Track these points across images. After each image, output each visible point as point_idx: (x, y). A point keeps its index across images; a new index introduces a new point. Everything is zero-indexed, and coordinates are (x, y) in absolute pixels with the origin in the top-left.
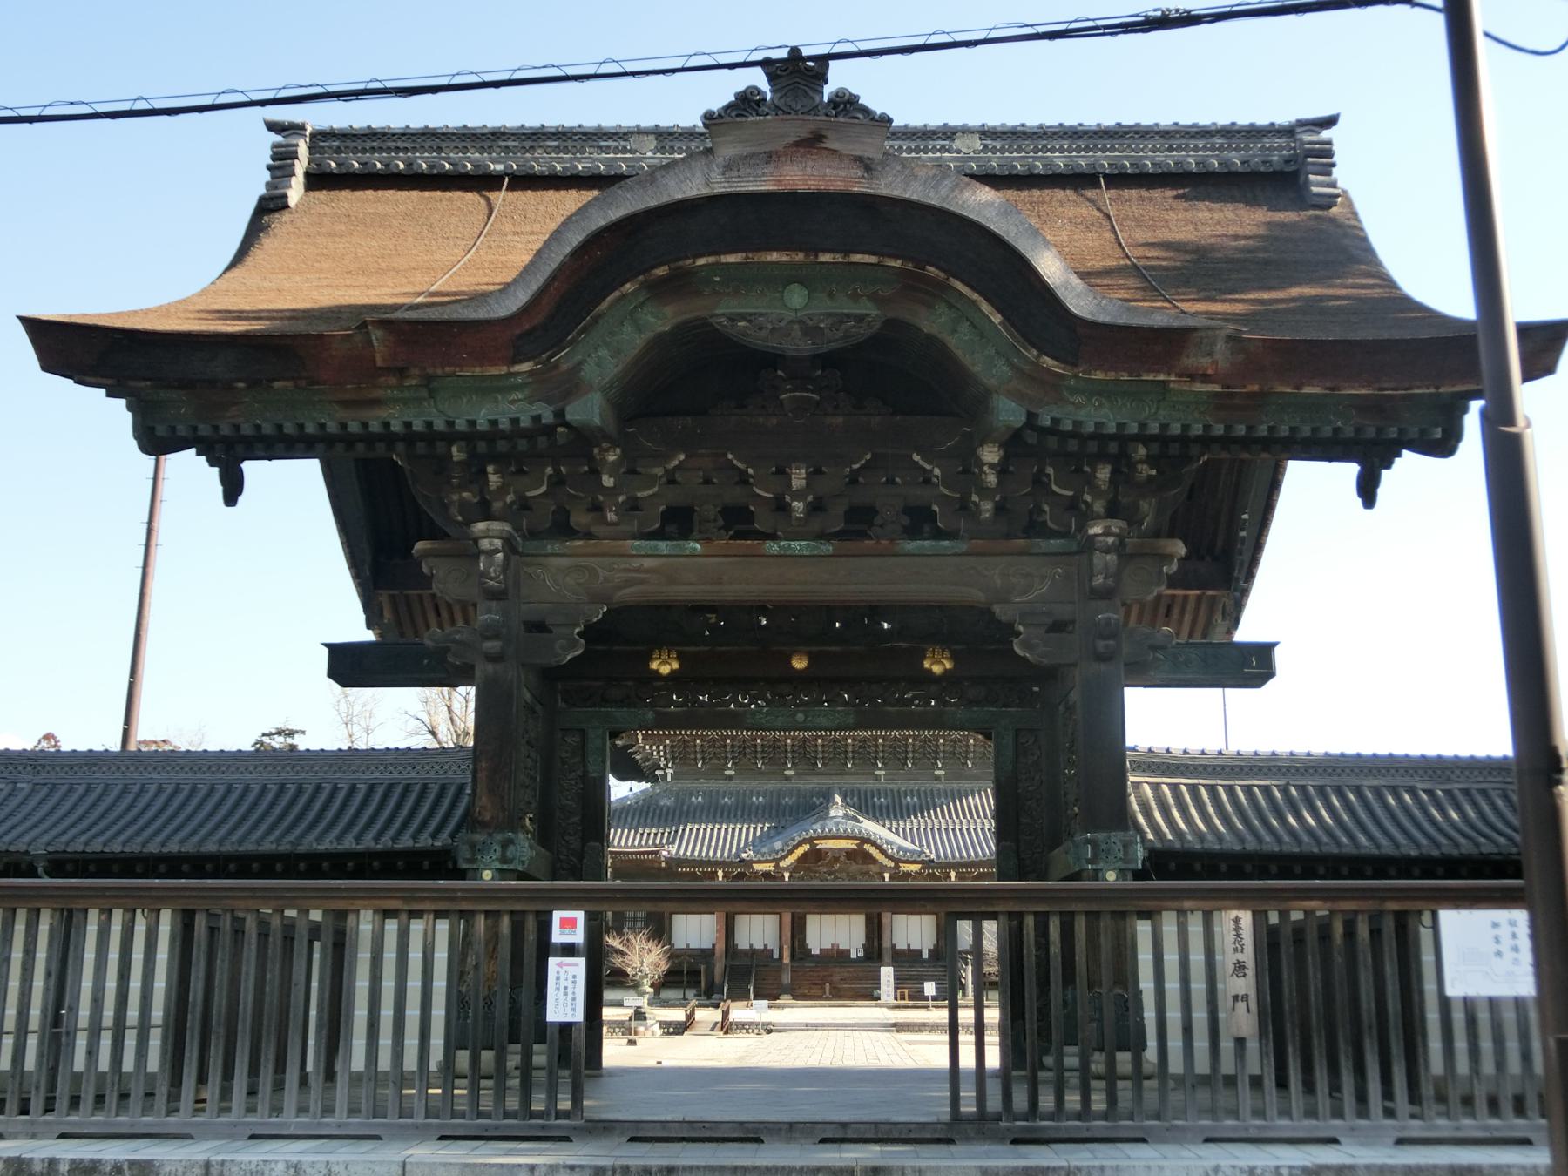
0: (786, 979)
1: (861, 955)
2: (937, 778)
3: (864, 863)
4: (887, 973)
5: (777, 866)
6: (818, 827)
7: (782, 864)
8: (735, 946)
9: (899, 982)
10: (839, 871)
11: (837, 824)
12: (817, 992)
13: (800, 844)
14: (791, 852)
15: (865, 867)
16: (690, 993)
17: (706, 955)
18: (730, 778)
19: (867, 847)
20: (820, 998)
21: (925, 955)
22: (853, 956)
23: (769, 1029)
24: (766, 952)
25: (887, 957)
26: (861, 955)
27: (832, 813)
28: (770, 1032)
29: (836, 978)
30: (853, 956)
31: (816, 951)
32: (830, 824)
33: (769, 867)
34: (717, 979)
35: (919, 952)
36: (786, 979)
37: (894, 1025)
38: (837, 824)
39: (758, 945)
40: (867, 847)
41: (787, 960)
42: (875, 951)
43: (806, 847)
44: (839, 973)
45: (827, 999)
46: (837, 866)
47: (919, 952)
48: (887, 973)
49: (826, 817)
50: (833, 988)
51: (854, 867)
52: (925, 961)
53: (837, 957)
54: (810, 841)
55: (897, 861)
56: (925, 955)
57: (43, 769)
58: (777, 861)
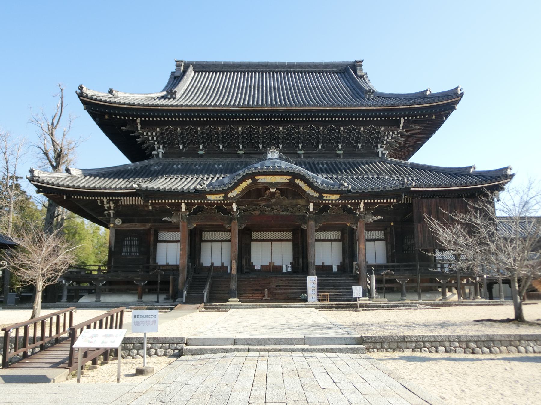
0: (234, 285)
1: (290, 269)
2: (338, 155)
3: (293, 198)
4: (312, 281)
5: (226, 197)
6: (258, 166)
7: (230, 195)
8: (200, 265)
9: (321, 287)
10: (275, 204)
11: (275, 163)
12: (258, 295)
13: (244, 179)
14: (236, 185)
15: (294, 202)
16: (162, 297)
17: (174, 269)
18: (202, 156)
19: (297, 181)
20: (261, 301)
21: (335, 269)
22: (284, 270)
23: (177, 349)
24: (223, 268)
25: (312, 270)
26: (290, 269)
27: (269, 156)
28: (180, 354)
29: (273, 286)
30: (284, 270)
31: (258, 267)
32: (267, 163)
33: (218, 197)
34: (180, 286)
35: (331, 267)
36: (234, 285)
37: (361, 341)
38: (275, 163)
39: (217, 264)
40: (297, 181)
41: (235, 272)
42: (302, 264)
43: (249, 181)
44: (275, 282)
45: (266, 301)
46: (273, 201)
47: (331, 267)
48: (312, 281)
49: (265, 159)
50: (271, 293)
51: (286, 202)
52: (335, 273)
53: (273, 271)
54: (251, 176)
55: (321, 192)
56: (335, 269)
57: (539, 364)
58: (225, 192)
